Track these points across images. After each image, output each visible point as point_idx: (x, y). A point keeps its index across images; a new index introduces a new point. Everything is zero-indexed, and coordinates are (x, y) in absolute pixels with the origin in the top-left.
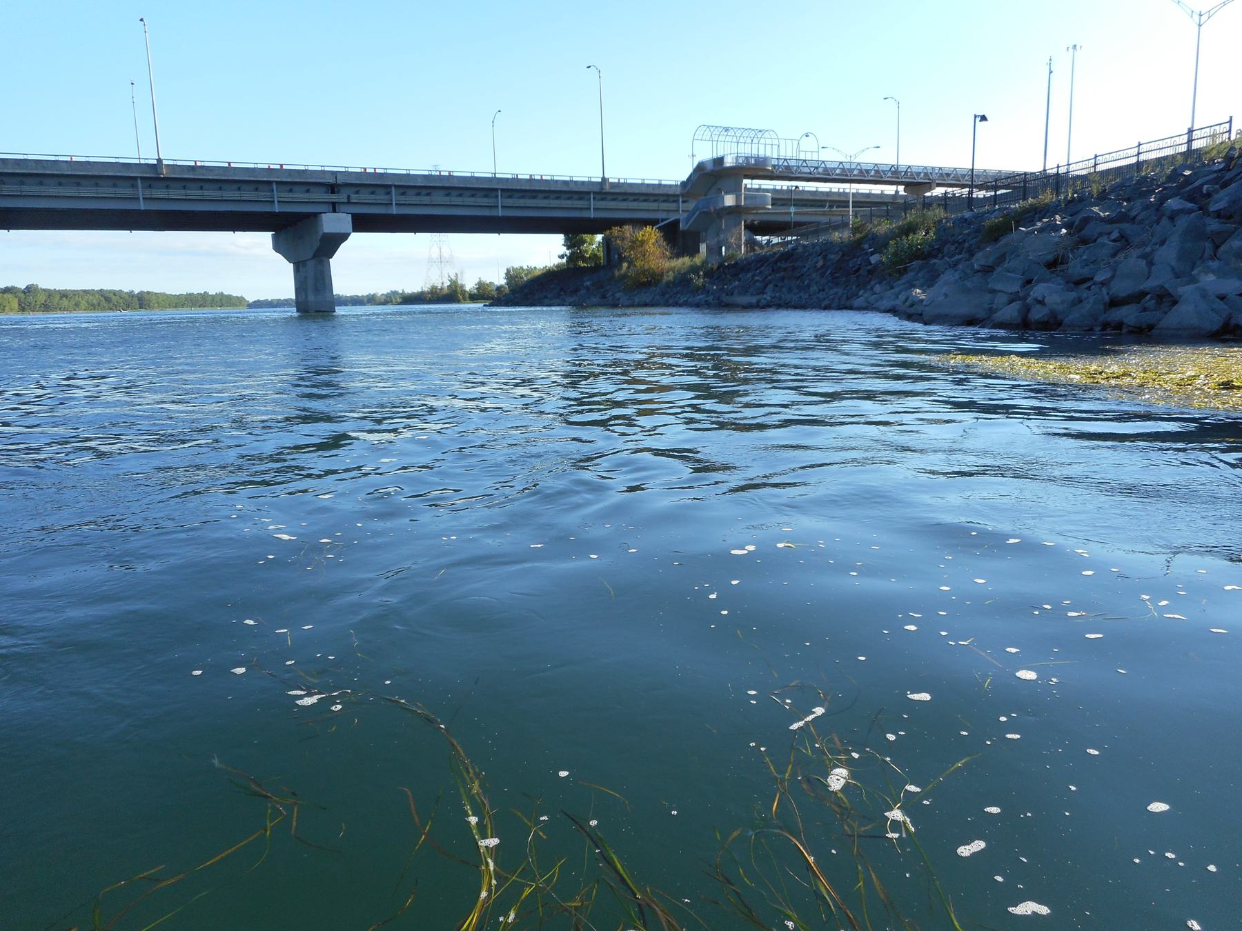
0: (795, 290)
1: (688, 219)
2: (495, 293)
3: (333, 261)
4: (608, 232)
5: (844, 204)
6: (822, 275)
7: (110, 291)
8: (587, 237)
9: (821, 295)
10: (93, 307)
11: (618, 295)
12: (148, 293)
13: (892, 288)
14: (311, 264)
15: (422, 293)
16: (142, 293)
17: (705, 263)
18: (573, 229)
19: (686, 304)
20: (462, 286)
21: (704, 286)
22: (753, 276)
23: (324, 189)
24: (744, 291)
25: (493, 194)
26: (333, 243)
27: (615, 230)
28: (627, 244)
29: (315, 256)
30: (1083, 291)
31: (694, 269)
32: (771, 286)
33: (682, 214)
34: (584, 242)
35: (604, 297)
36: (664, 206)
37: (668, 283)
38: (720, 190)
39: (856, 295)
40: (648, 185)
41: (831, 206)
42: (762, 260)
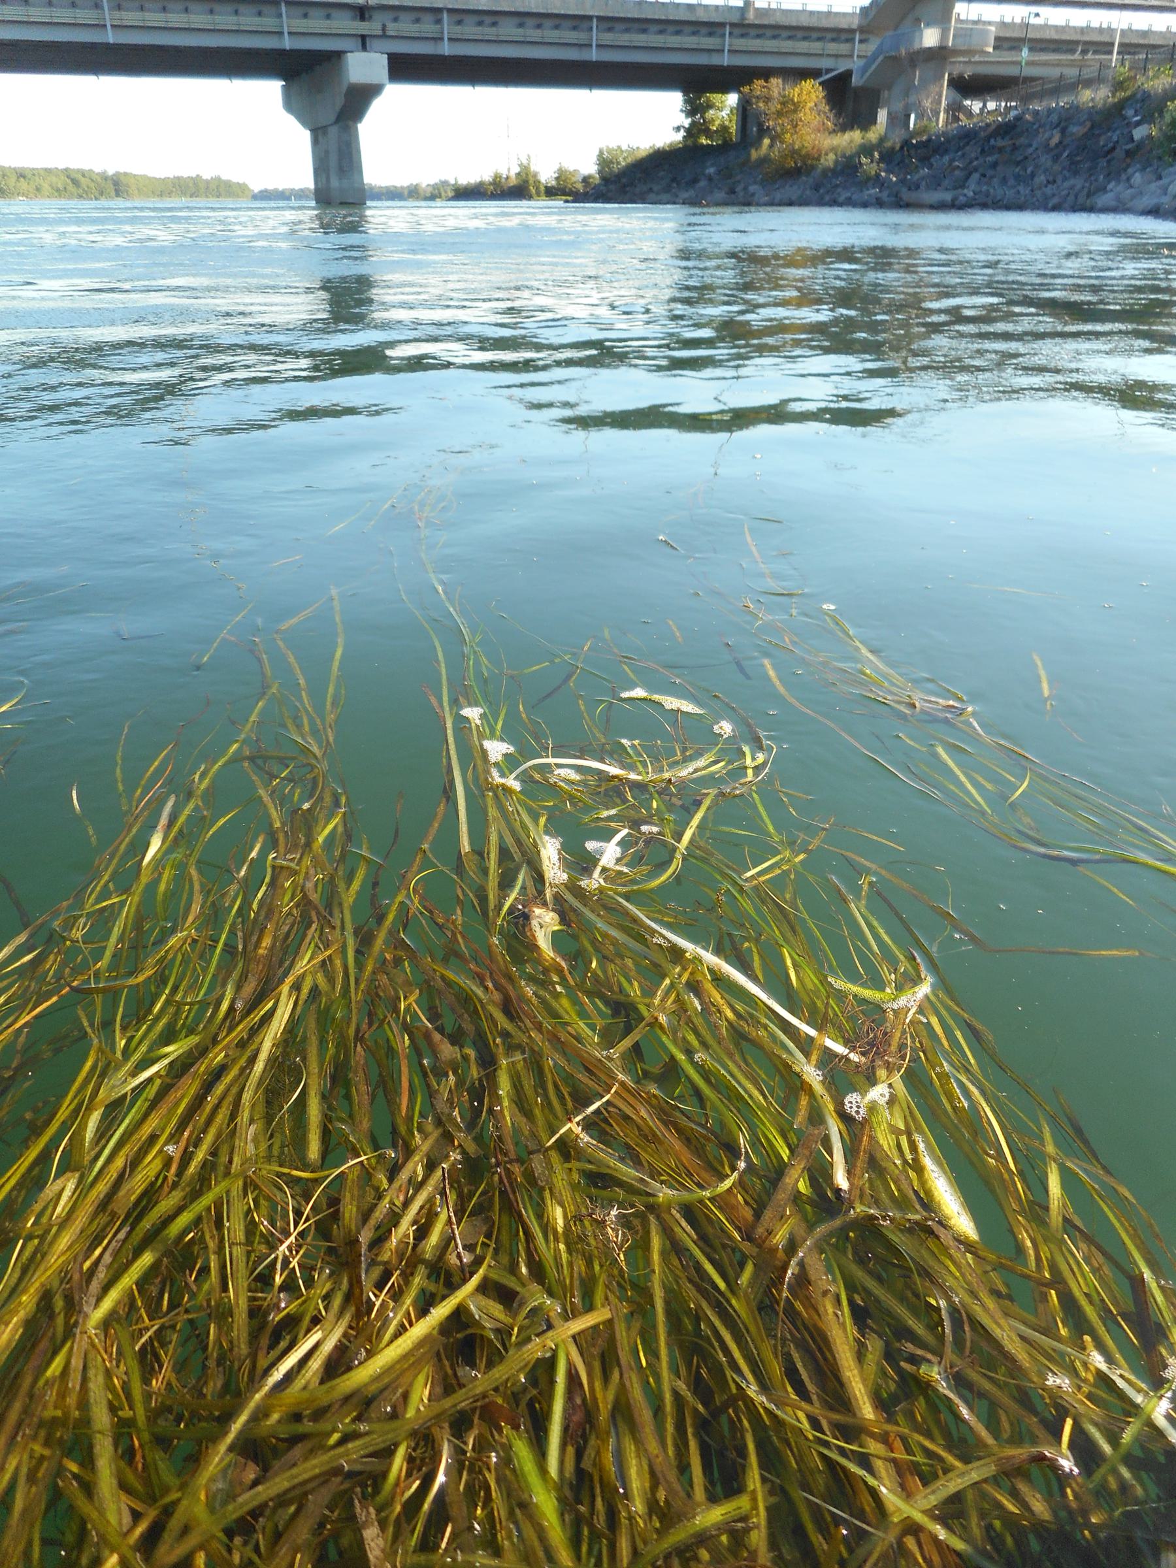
0: (1011, 182)
1: (864, 69)
2: (580, 187)
3: (360, 126)
4: (746, 89)
5: (1105, 47)
6: (1056, 158)
7: (78, 171)
8: (716, 98)
9: (1048, 190)
10: (60, 192)
11: (752, 188)
12: (126, 174)
13: (1160, 178)
14: (333, 131)
15: (481, 184)
16: (117, 174)
17: (882, 140)
18: (697, 83)
19: (850, 203)
20: (535, 175)
21: (878, 175)
22: (952, 160)
23: (348, 14)
24: (936, 183)
25: (585, 25)
26: (359, 99)
27: (758, 84)
28: (775, 106)
29: (338, 120)
30: (376, 1272)
31: (866, 150)
32: (976, 176)
33: (856, 60)
34: (710, 106)
35: (732, 191)
36: (832, 47)
37: (825, 172)
38: (918, 21)
39: (1104, 189)
40: (812, 13)
41: (1084, 52)
42: (967, 136)
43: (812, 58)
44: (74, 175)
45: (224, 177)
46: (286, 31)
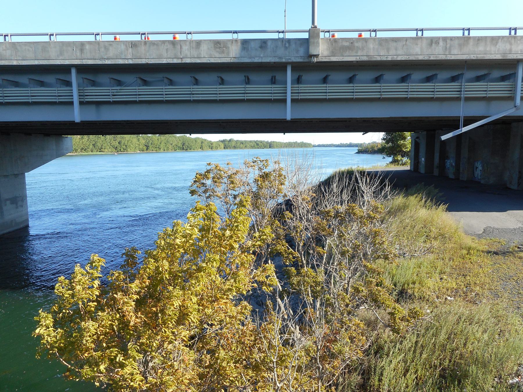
40: (433, 41)
43: (446, 104)
44: (258, 142)
45: (304, 142)
46: (76, 100)
